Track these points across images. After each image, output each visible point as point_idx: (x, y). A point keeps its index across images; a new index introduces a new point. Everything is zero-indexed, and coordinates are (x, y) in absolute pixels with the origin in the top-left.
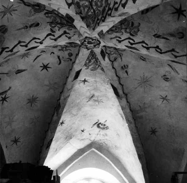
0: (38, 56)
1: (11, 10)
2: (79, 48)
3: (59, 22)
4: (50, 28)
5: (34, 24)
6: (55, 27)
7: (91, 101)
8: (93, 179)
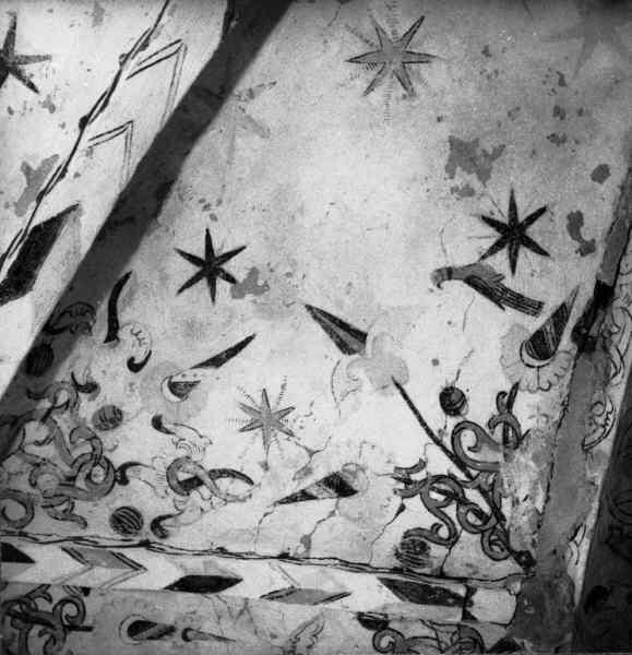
0: (216, 362)
3: (36, 629)
4: (85, 599)
5: (151, 638)
6: (63, 602)
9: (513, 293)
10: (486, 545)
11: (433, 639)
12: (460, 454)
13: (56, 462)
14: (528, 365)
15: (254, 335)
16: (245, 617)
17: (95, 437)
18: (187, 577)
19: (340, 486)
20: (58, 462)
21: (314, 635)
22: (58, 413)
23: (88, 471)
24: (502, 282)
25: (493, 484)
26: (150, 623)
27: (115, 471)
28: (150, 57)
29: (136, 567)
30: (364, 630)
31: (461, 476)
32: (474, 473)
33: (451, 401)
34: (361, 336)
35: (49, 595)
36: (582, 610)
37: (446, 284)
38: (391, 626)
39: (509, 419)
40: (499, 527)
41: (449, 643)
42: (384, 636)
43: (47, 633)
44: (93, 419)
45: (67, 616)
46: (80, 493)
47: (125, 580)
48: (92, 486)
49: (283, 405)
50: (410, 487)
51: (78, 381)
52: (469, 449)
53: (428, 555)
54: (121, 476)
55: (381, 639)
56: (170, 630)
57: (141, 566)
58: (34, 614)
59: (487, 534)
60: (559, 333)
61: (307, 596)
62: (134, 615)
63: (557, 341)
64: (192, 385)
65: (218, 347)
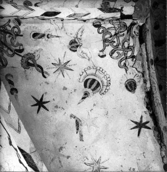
1: (58, 67)
2: (141, 72)
3: (8, 35)
4: (20, 27)
5: (39, 38)
6: (14, 27)
8: (12, 146)
11: (113, 27)
16: (63, 29)
18: (46, 12)
21: (82, 32)
26: (38, 33)
28: (19, 155)
29: (32, 10)
36: (152, 8)
38: (102, 26)
41: (118, 28)
43: (11, 36)
45: (15, 32)
47: (30, 13)
53: (110, 5)
56: (43, 35)
57: (33, 10)
58: (6, 31)
61: (79, 15)
62: (33, 31)
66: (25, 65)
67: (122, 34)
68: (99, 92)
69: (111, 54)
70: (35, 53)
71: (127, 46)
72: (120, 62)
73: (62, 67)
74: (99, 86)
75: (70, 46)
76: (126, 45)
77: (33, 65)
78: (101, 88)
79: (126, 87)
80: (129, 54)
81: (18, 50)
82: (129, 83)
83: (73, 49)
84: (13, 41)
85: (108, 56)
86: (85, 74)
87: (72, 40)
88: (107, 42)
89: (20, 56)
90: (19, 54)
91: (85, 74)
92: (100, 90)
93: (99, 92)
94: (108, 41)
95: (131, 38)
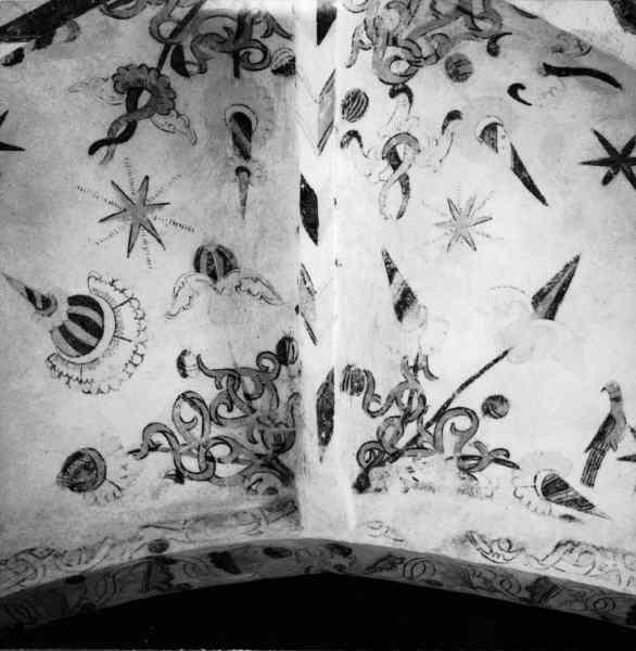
0: (519, 168)
1: (136, 198)
5: (234, 136)
6: (265, 50)
7: (577, 493)
9: (600, 460)
10: (368, 446)
12: (446, 416)
13: (412, 24)
14: (536, 477)
15: (547, 205)
17: (438, 58)
19: (404, 303)
20: (413, 26)
22: (465, 20)
23: (403, 57)
24: (611, 450)
25: (423, 448)
26: (250, 135)
27: (403, 83)
30: (276, 342)
31: (427, 417)
32: (431, 429)
33: (495, 406)
34: (551, 315)
35: (270, 35)
37: (606, 396)
38: (283, 368)
39: (484, 460)
40: (386, 455)
42: (273, 362)
44: (457, 55)
45: (249, 53)
46: (381, 53)
48: (388, 63)
49: (477, 239)
50: (411, 371)
51: (502, 39)
52: (453, 424)
54: (399, 89)
55: (271, 359)
56: (246, 155)
59: (378, 446)
60: (568, 504)
63: (560, 502)
64: (494, 146)
65: (532, 170)
66: (129, 77)
67: (257, 436)
68: (53, 350)
69: (189, 395)
70: (179, 115)
71: (214, 455)
72: (163, 428)
73: (137, 214)
74: (77, 350)
75: (212, 249)
76: (219, 451)
77: (132, 105)
78: (73, 360)
79: (78, 455)
80: (191, 464)
81: (183, 57)
82: (92, 466)
83: (204, 261)
84: (214, 44)
85: (183, 385)
86: (118, 298)
87: (232, 256)
88: (231, 383)
89: (161, 62)
90: (168, 59)
91: (118, 298)
92: (64, 356)
93: (53, 350)
94: (233, 385)
95: (241, 467)
